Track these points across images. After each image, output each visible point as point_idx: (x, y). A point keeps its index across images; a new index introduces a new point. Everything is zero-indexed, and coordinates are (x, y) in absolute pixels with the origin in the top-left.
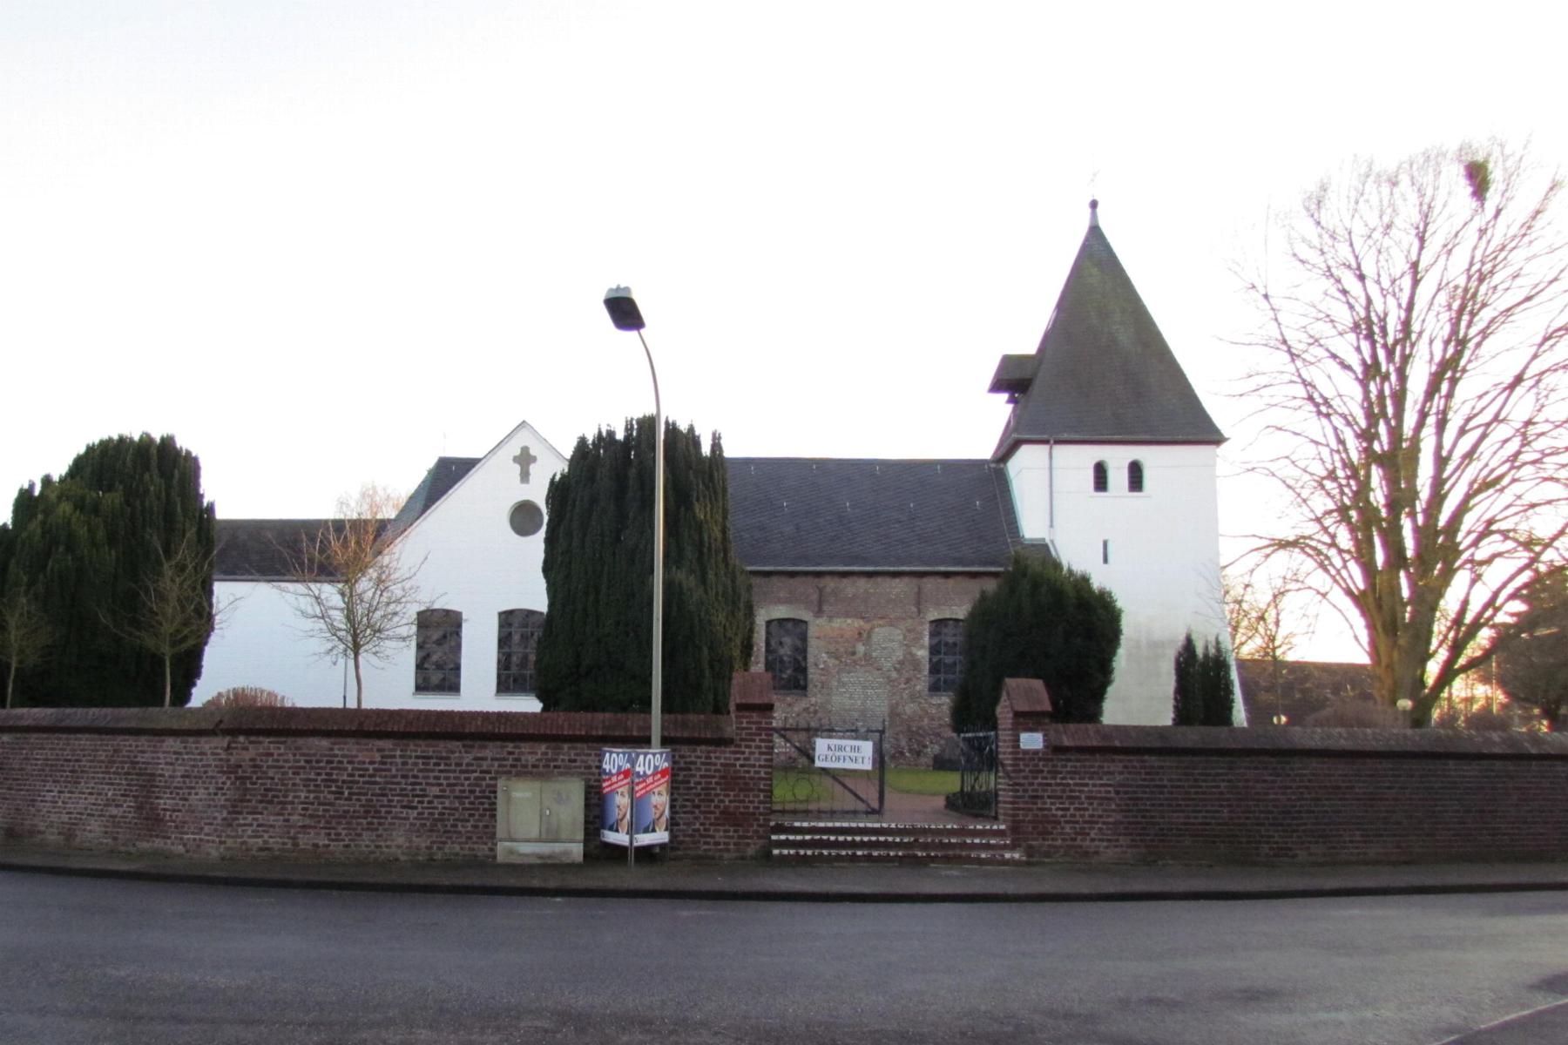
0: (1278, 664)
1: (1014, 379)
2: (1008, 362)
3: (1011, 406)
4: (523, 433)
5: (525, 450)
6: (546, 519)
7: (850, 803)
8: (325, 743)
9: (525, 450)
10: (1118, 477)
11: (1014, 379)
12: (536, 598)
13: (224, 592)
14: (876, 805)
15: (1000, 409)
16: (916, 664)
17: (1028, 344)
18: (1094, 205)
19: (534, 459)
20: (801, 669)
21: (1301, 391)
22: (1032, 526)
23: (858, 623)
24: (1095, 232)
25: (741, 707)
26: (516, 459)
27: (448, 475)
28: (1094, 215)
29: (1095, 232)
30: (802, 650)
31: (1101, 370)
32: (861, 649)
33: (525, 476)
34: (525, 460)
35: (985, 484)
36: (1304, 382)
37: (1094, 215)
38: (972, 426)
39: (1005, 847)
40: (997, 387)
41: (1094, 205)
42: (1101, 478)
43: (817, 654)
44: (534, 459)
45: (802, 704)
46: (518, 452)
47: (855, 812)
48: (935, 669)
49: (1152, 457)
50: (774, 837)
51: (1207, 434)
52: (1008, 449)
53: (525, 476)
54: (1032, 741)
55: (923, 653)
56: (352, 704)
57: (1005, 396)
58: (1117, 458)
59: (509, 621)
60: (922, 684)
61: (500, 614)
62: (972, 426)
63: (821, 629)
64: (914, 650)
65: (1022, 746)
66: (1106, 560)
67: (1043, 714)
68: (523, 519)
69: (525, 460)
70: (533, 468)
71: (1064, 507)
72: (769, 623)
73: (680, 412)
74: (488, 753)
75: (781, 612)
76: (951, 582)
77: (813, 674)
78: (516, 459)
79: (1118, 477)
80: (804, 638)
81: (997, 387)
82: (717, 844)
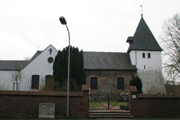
0: (168, 85)
1: (130, 40)
2: (129, 37)
3: (130, 45)
4: (51, 46)
5: (51, 49)
6: (54, 60)
7: (103, 108)
8: (8, 97)
9: (51, 49)
10: (146, 56)
11: (130, 40)
12: (51, 73)
13: (52, 74)
14: (107, 108)
15: (128, 45)
16: (115, 84)
17: (132, 35)
18: (142, 15)
19: (52, 50)
20: (96, 85)
21: (173, 43)
22: (133, 63)
23: (106, 78)
24: (142, 19)
25: (83, 91)
26: (49, 50)
27: (39, 52)
28: (142, 17)
29: (142, 19)
30: (96, 82)
31: (143, 39)
32: (106, 82)
33: (51, 53)
34: (51, 51)
35: (126, 56)
36: (173, 41)
37: (142, 17)
38: (124, 47)
39: (130, 115)
40: (127, 41)
41: (142, 15)
42: (144, 56)
43: (99, 83)
44: (52, 50)
45: (97, 91)
46: (49, 49)
47: (104, 109)
48: (118, 85)
49: (152, 53)
50: (89, 114)
51: (161, 50)
52: (129, 51)
53: (51, 53)
54: (134, 97)
55: (116, 83)
56: (15, 90)
57: (129, 43)
58: (146, 53)
59: (48, 77)
60: (116, 88)
61: (33, 76)
62: (124, 47)
63: (99, 79)
64: (115, 82)
65: (133, 98)
66: (145, 66)
67: (136, 92)
68: (50, 60)
69: (51, 51)
70: (52, 52)
71: (138, 60)
72: (91, 78)
73: (74, 45)
74: (38, 99)
75: (93, 76)
76: (120, 72)
77: (98, 86)
78: (49, 50)
79: (146, 56)
80: (97, 81)
81: (127, 41)
82: (79, 115)
